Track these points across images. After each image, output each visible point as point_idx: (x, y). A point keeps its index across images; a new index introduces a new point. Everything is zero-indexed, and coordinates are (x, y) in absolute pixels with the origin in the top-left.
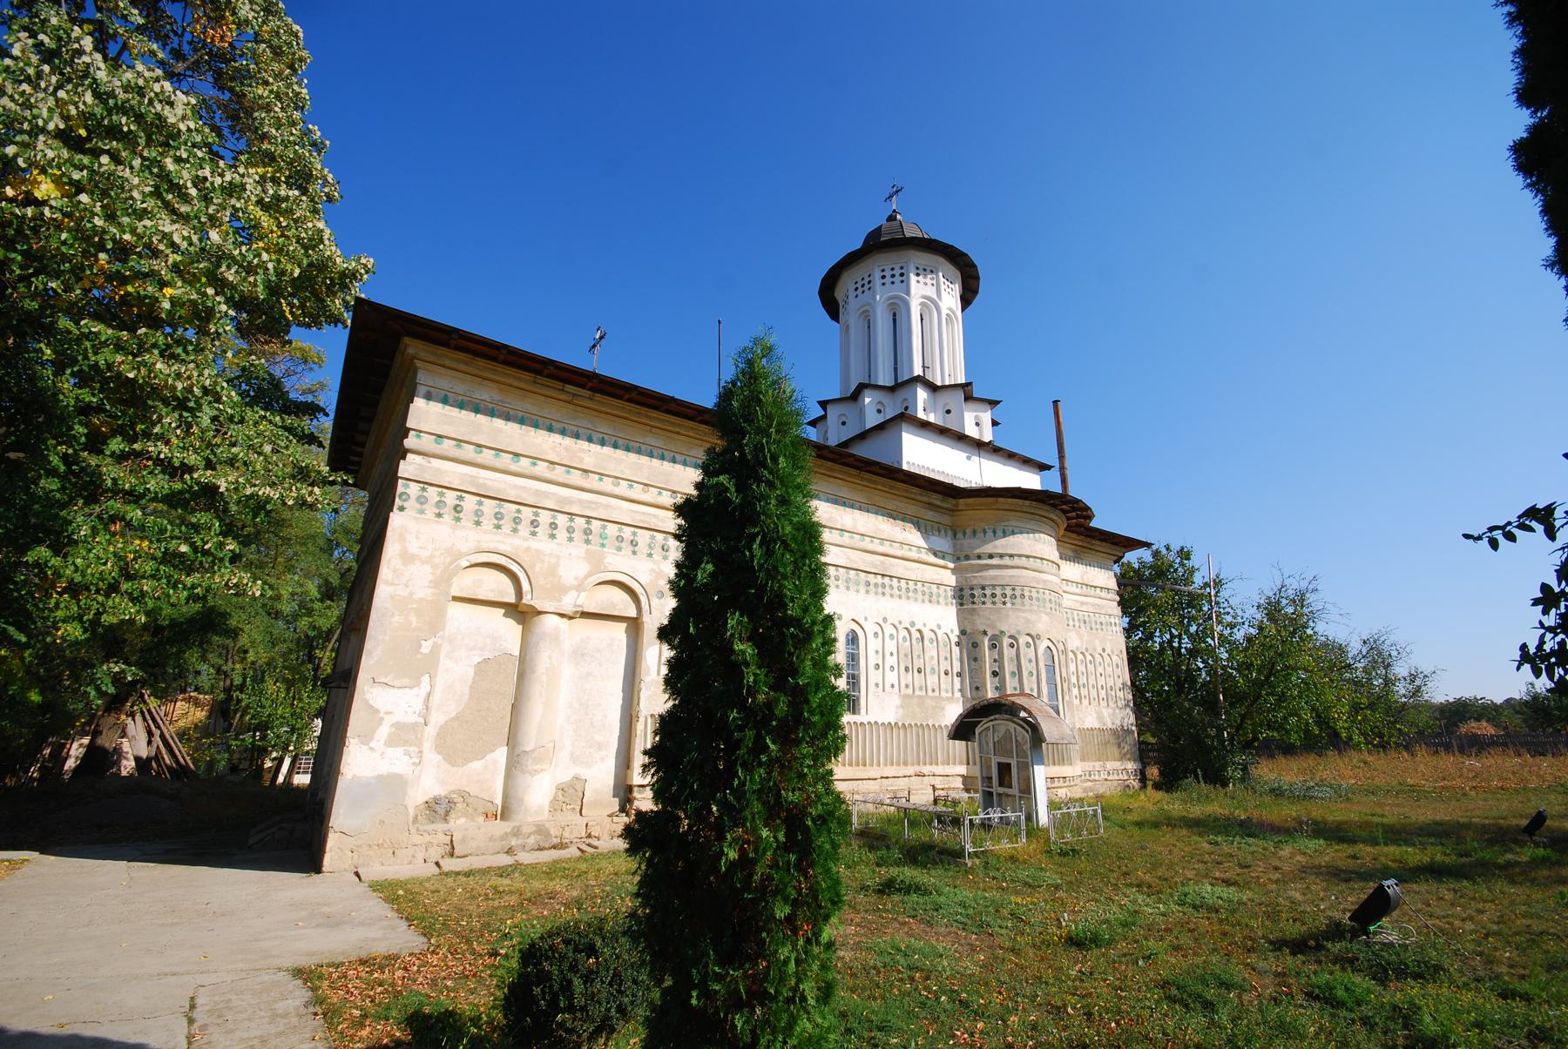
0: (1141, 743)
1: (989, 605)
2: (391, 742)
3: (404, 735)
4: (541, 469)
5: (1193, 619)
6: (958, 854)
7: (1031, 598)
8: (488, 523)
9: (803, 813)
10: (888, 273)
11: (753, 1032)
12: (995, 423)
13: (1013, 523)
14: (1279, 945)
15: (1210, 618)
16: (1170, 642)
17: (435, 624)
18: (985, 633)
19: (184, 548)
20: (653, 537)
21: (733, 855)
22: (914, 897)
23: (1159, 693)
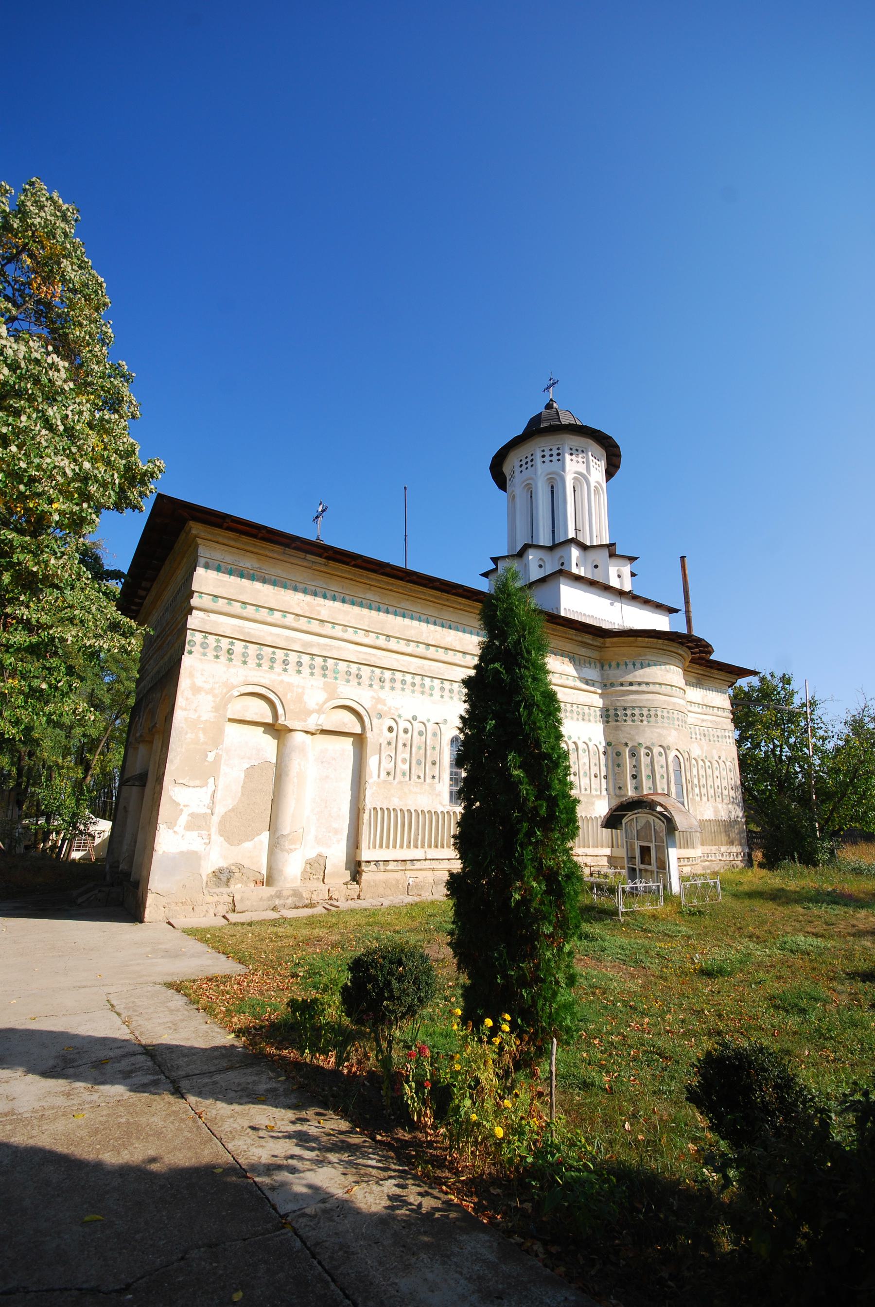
0: (750, 831)
1: (629, 722)
2: (189, 827)
3: (197, 822)
4: (290, 620)
5: (791, 732)
6: (613, 913)
7: (663, 717)
8: (252, 662)
9: (557, 874)
10: (547, 453)
11: (533, 997)
12: (633, 575)
13: (648, 657)
14: (852, 976)
15: (806, 732)
16: (773, 751)
17: (217, 740)
18: (626, 744)
19: (44, 686)
20: (373, 672)
21: (518, 897)
22: (585, 942)
23: (764, 792)
